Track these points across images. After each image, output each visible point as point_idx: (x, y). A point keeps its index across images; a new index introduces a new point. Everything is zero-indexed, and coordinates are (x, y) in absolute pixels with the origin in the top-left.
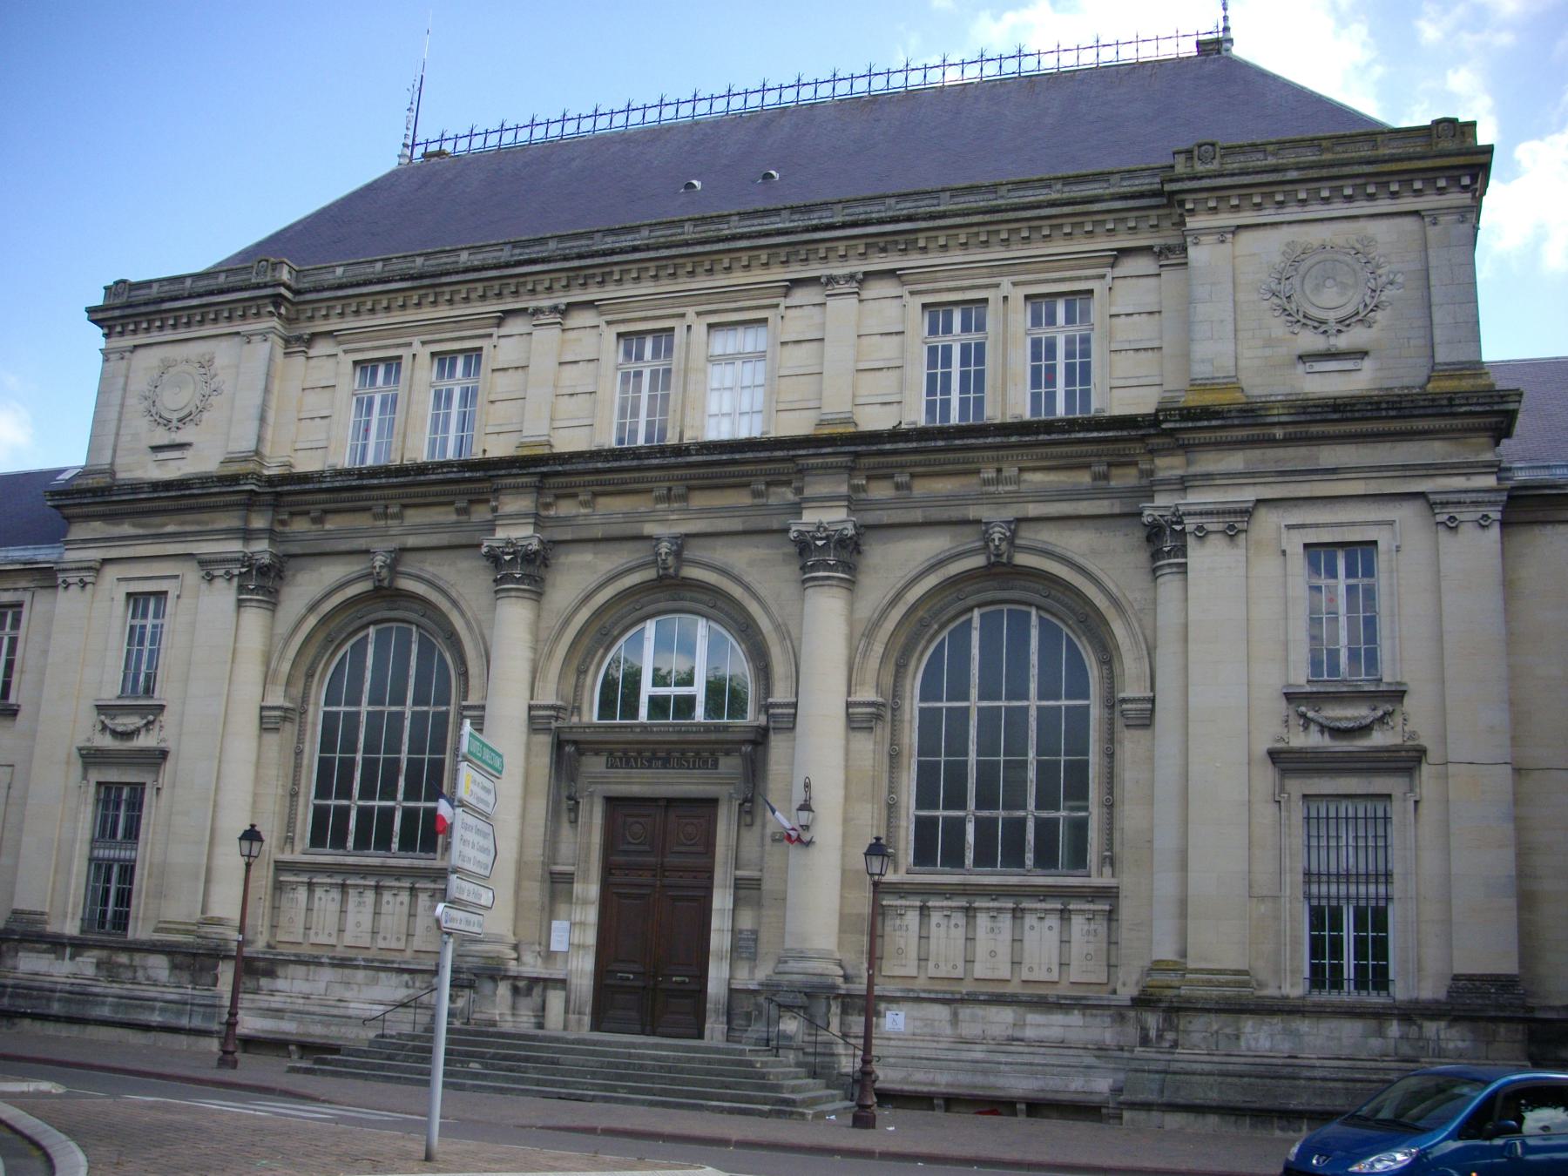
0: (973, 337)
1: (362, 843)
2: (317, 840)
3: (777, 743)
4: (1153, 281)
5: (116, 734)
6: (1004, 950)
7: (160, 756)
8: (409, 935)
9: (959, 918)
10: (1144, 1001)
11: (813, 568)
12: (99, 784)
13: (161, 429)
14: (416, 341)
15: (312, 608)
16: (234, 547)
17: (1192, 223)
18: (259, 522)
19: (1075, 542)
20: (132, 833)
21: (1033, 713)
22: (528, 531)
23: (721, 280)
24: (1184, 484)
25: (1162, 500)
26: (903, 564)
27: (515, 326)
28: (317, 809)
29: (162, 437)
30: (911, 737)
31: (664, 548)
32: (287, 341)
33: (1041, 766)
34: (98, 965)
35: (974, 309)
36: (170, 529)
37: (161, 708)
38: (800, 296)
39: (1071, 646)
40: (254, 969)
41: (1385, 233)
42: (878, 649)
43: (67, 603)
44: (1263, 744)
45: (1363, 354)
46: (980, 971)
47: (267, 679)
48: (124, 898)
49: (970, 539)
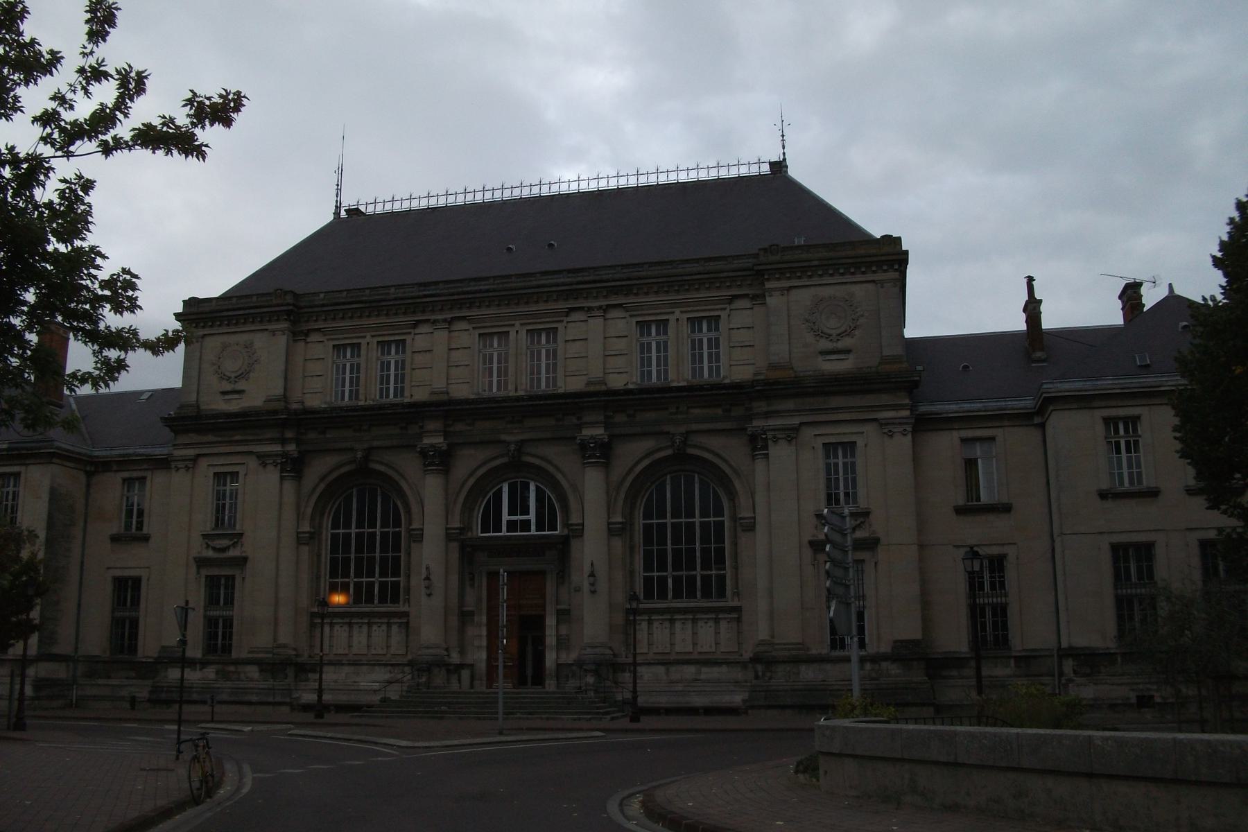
3: (575, 544)
4: (749, 312)
5: (214, 549)
6: (364, 641)
7: (242, 561)
8: (388, 647)
9: (667, 624)
10: (756, 659)
11: (590, 457)
12: (207, 577)
13: (224, 383)
14: (368, 335)
15: (322, 479)
16: (277, 448)
17: (768, 285)
18: (289, 434)
19: (715, 443)
20: (230, 602)
21: (697, 525)
22: (441, 440)
23: (534, 308)
24: (767, 415)
25: (755, 423)
26: (633, 454)
27: (424, 329)
28: (646, 578)
30: (639, 537)
31: (512, 447)
32: (294, 334)
33: (703, 550)
34: (217, 673)
36: (237, 438)
37: (241, 535)
38: (575, 316)
39: (715, 493)
41: (861, 292)
42: (622, 495)
43: (179, 479)
44: (807, 537)
45: (848, 351)
46: (678, 649)
47: (299, 516)
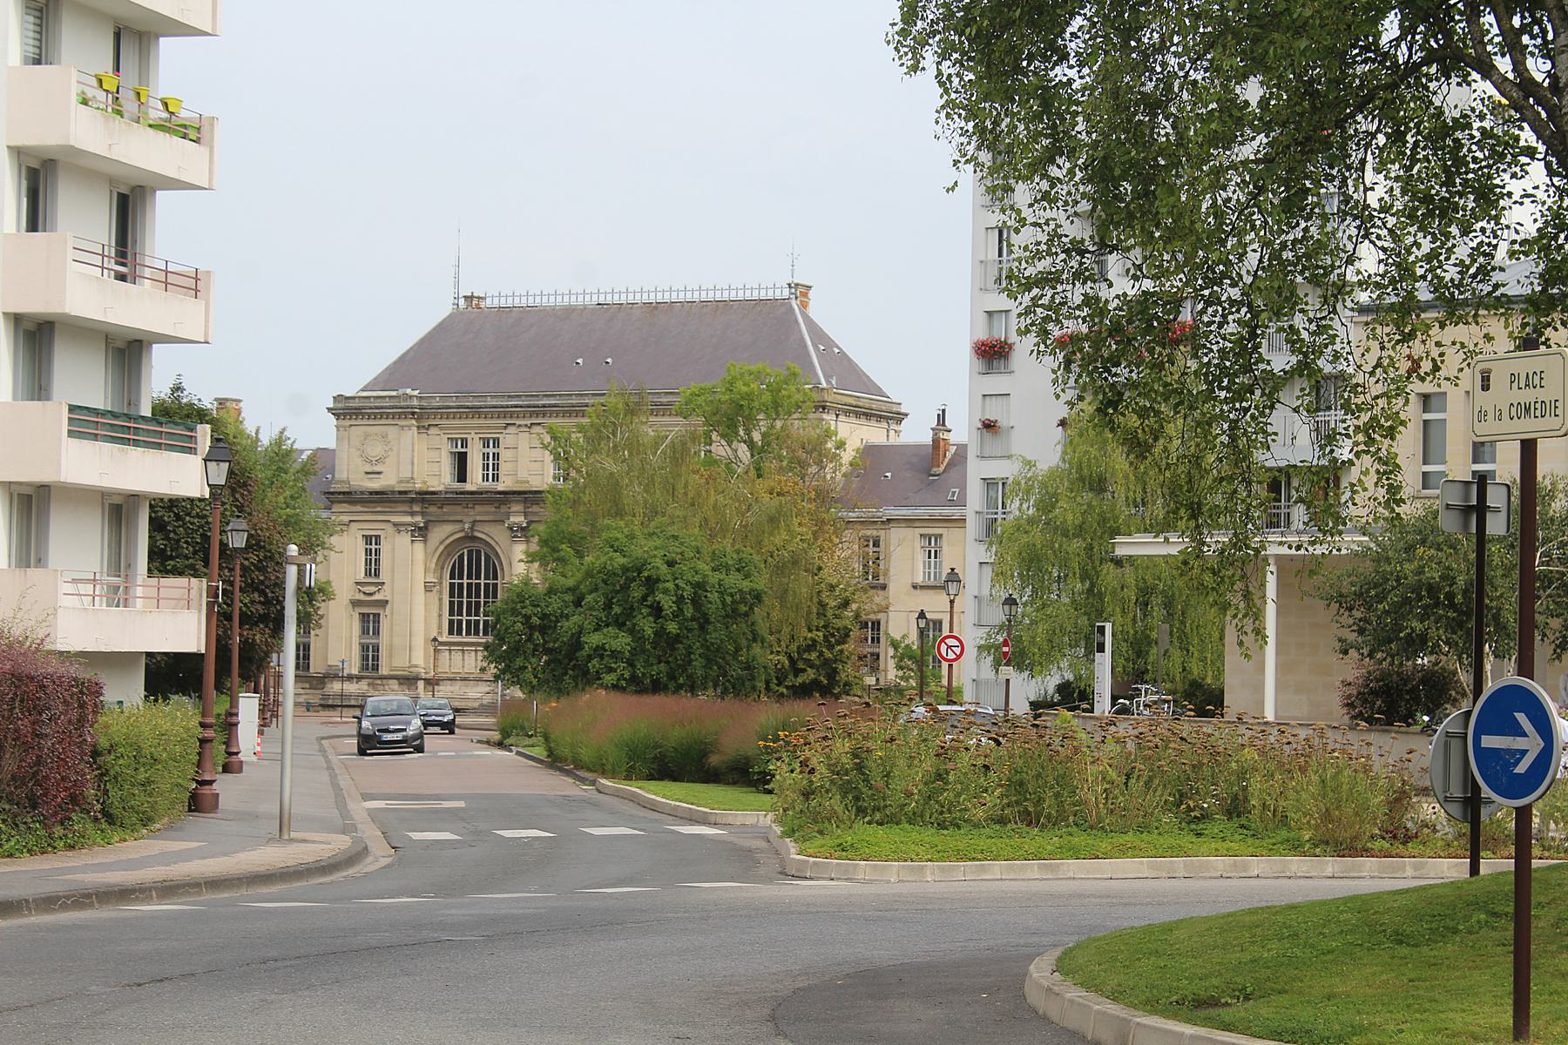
1: (468, 633)
2: (451, 632)
16: (408, 519)
18: (416, 508)
19: (487, 528)
26: (442, 534)
27: (511, 430)
40: (431, 683)
48: (376, 658)
49: (457, 527)
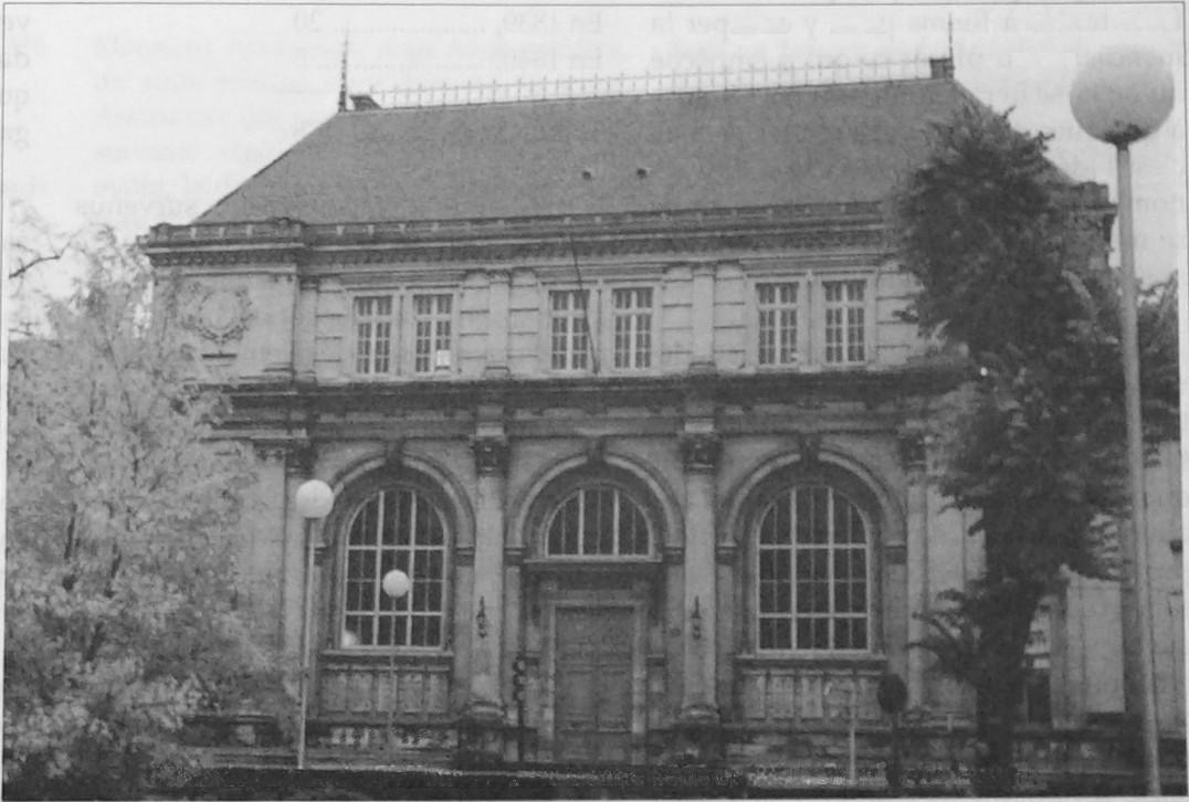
0: (856, 304)
9: (789, 681)
16: (283, 435)
26: (533, 464)
29: (212, 348)
31: (593, 445)
35: (789, 290)
38: (675, 273)
